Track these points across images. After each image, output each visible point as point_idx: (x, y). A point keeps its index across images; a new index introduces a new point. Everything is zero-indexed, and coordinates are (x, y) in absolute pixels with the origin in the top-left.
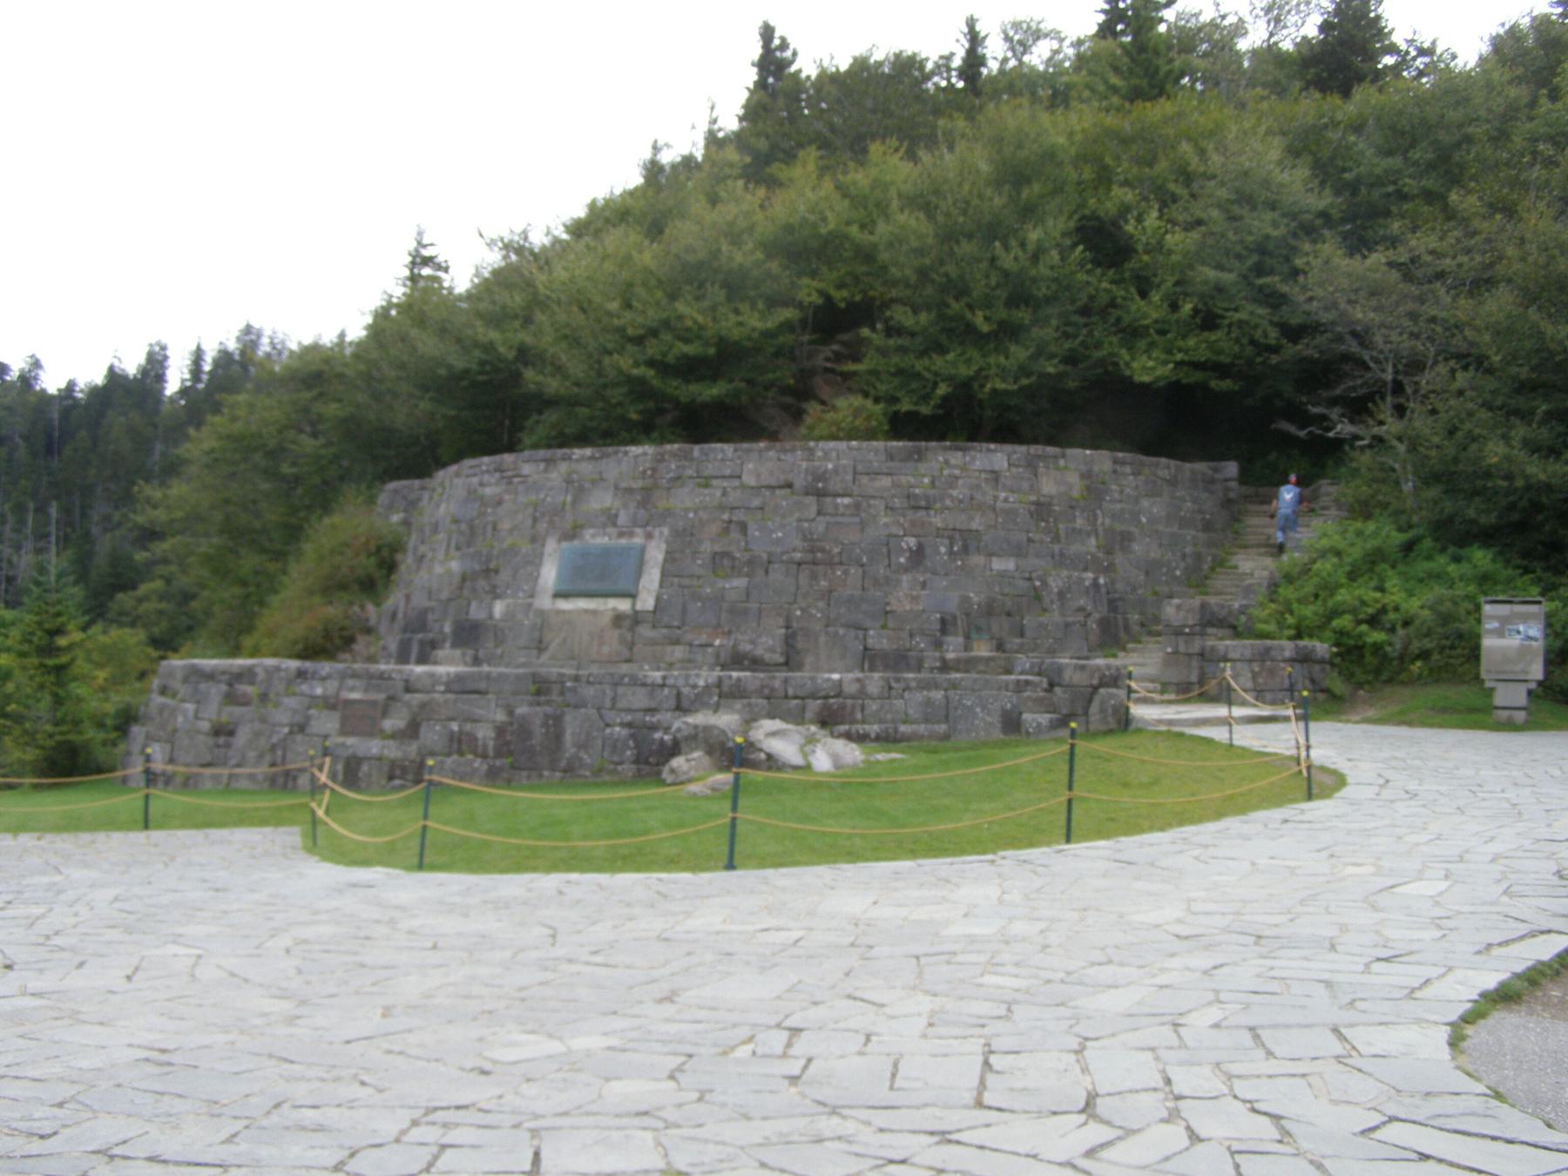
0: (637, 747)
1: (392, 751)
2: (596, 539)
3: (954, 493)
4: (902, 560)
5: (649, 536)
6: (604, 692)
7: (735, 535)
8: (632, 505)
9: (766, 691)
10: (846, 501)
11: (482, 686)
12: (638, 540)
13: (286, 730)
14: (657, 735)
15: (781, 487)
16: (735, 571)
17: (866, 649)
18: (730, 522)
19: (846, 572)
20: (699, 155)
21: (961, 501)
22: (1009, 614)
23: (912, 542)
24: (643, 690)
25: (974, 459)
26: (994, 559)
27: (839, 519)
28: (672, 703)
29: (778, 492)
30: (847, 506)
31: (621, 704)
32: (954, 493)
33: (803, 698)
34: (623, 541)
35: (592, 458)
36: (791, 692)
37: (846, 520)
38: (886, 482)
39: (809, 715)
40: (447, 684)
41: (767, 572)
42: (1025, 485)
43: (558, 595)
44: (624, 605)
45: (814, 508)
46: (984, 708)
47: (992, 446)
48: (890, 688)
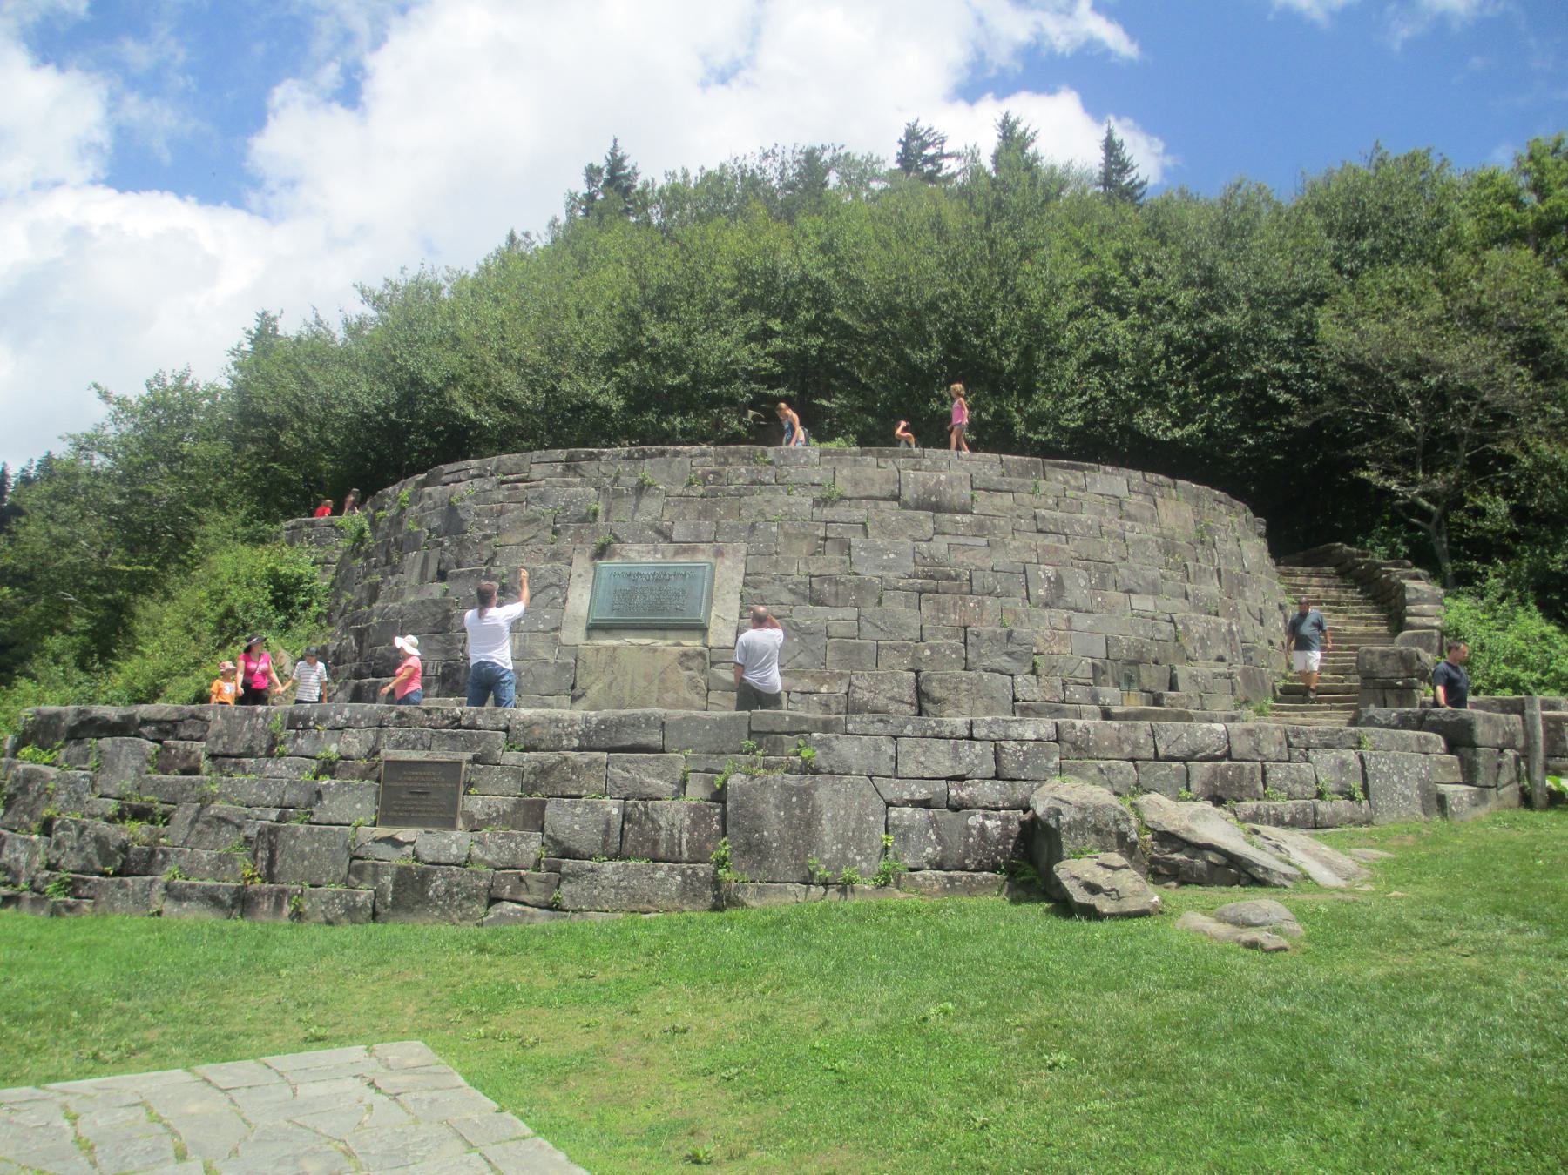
0: (940, 840)
1: (492, 847)
2: (640, 556)
3: (1083, 517)
4: (1041, 592)
5: (719, 553)
6: (877, 749)
7: (833, 556)
8: (691, 516)
9: (1127, 748)
10: (967, 518)
11: (655, 738)
12: (703, 558)
13: (274, 814)
14: (975, 820)
15: (884, 499)
16: (839, 600)
17: (1015, 700)
18: (826, 539)
19: (980, 604)
20: (990, 95)
21: (1090, 528)
22: (1156, 662)
23: (1050, 571)
24: (942, 746)
25: (1094, 480)
26: (1133, 596)
27: (962, 540)
28: (989, 767)
29: (882, 504)
30: (969, 525)
31: (908, 768)
32: (1083, 517)
33: (1184, 760)
34: (683, 560)
35: (630, 457)
36: (1161, 752)
37: (970, 541)
38: (1007, 499)
39: (1196, 786)
40: (585, 735)
41: (880, 603)
42: (1147, 514)
43: (594, 628)
44: (692, 643)
45: (929, 526)
46: (1402, 776)
47: (1109, 469)
48: (1290, 745)
